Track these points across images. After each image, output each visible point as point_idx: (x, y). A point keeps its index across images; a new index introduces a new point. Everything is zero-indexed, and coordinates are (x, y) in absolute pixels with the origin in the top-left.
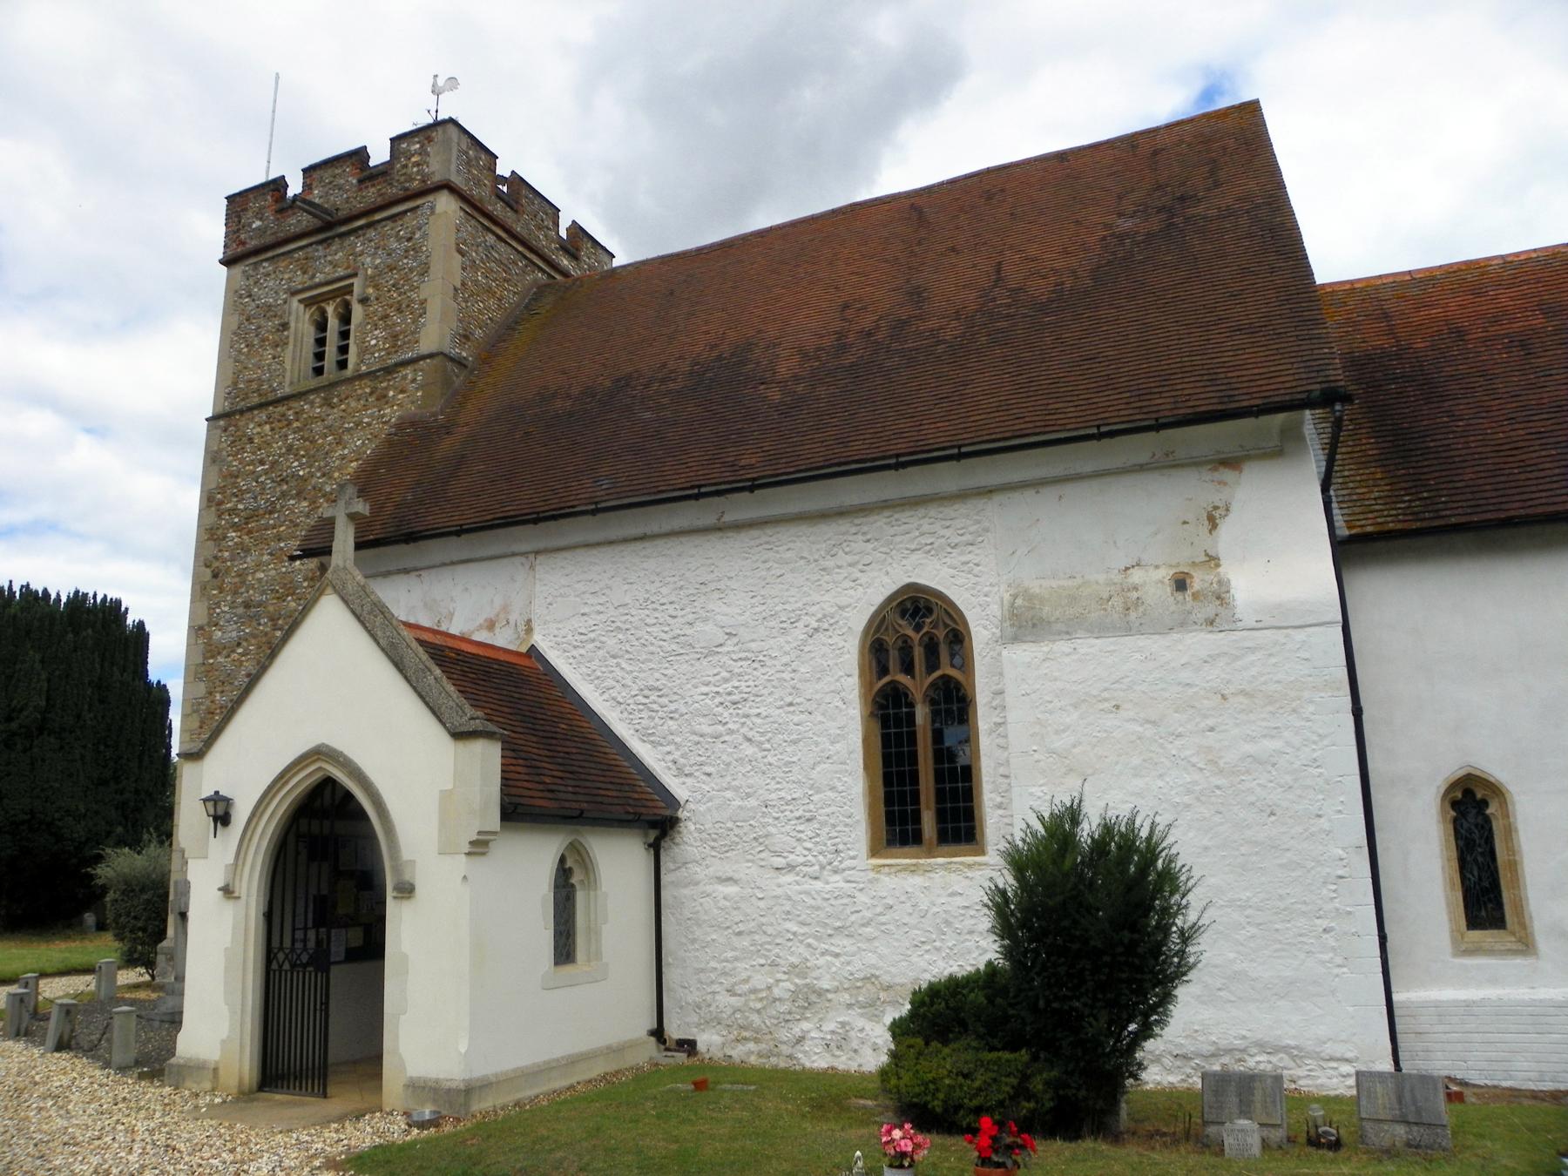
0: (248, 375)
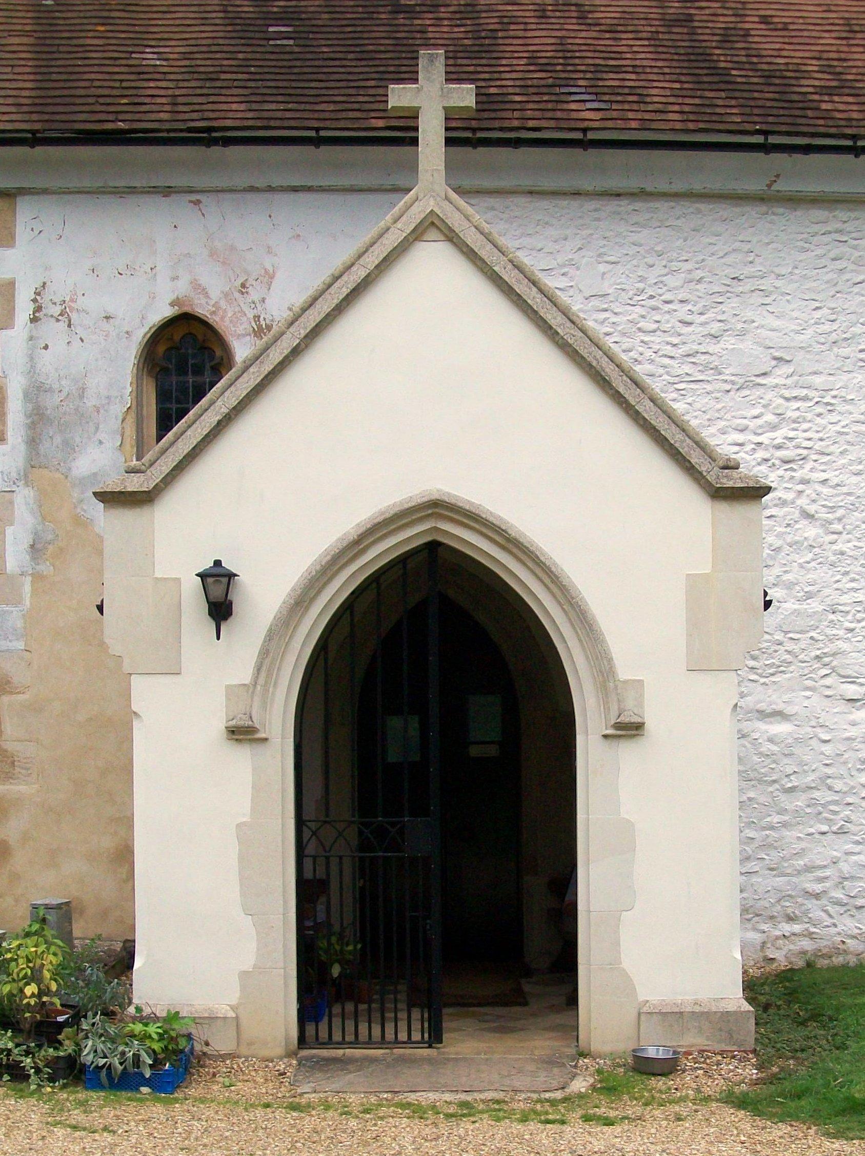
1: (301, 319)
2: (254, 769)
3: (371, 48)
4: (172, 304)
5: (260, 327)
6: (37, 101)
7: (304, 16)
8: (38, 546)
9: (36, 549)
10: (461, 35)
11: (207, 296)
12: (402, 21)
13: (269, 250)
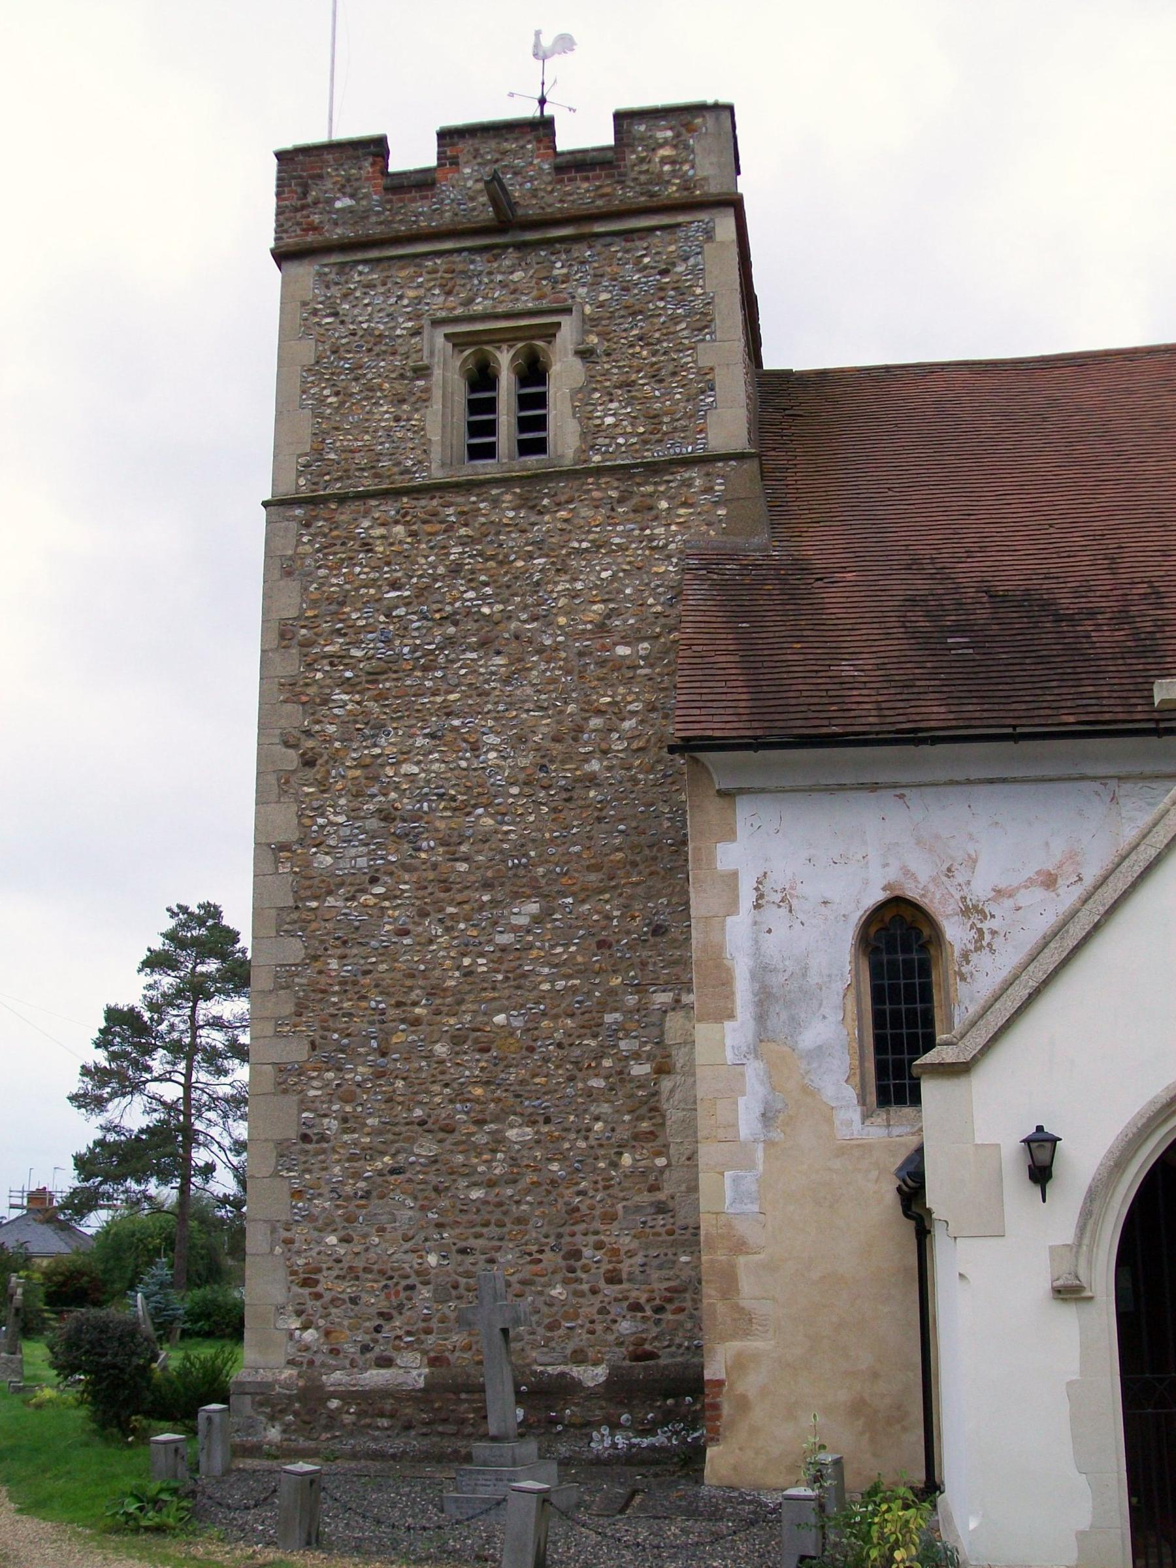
0: (342, 440)
1: (1096, 897)
2: (1081, 1328)
3: (1045, 653)
4: (884, 889)
5: (967, 907)
6: (754, 710)
7: (976, 628)
8: (770, 1115)
9: (767, 1118)
10: (1123, 638)
11: (916, 880)
12: (1065, 629)
13: (971, 837)
